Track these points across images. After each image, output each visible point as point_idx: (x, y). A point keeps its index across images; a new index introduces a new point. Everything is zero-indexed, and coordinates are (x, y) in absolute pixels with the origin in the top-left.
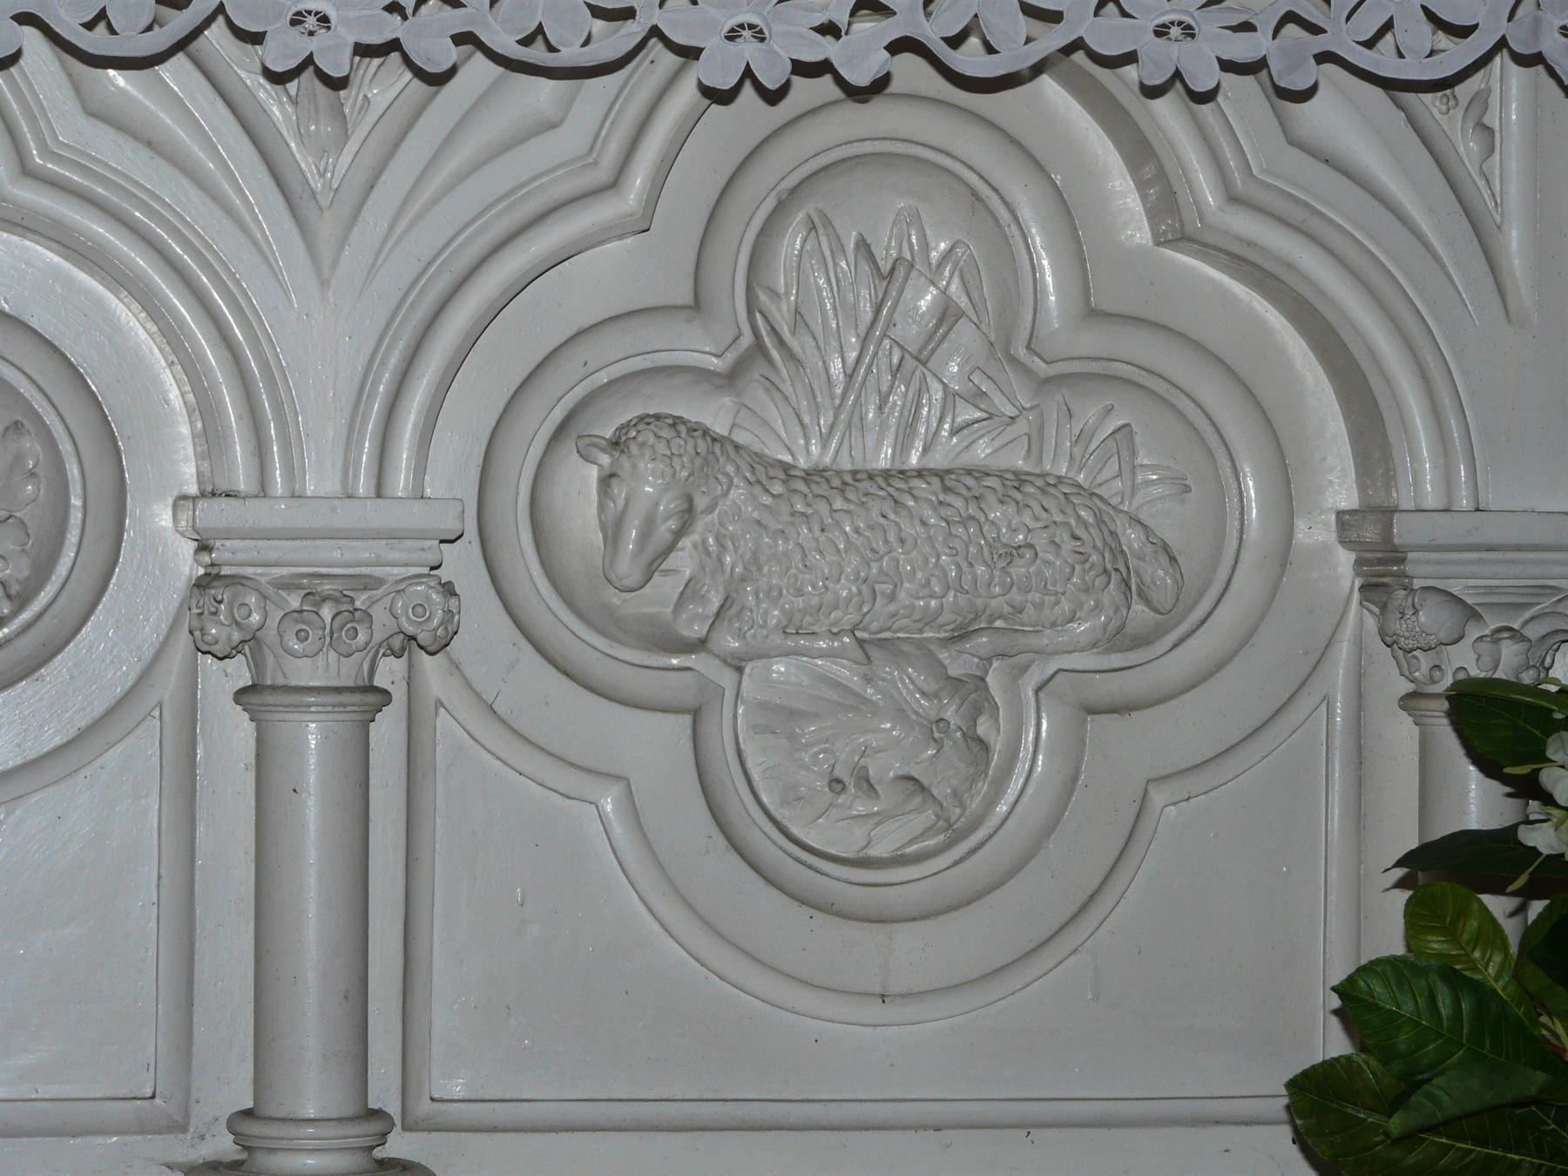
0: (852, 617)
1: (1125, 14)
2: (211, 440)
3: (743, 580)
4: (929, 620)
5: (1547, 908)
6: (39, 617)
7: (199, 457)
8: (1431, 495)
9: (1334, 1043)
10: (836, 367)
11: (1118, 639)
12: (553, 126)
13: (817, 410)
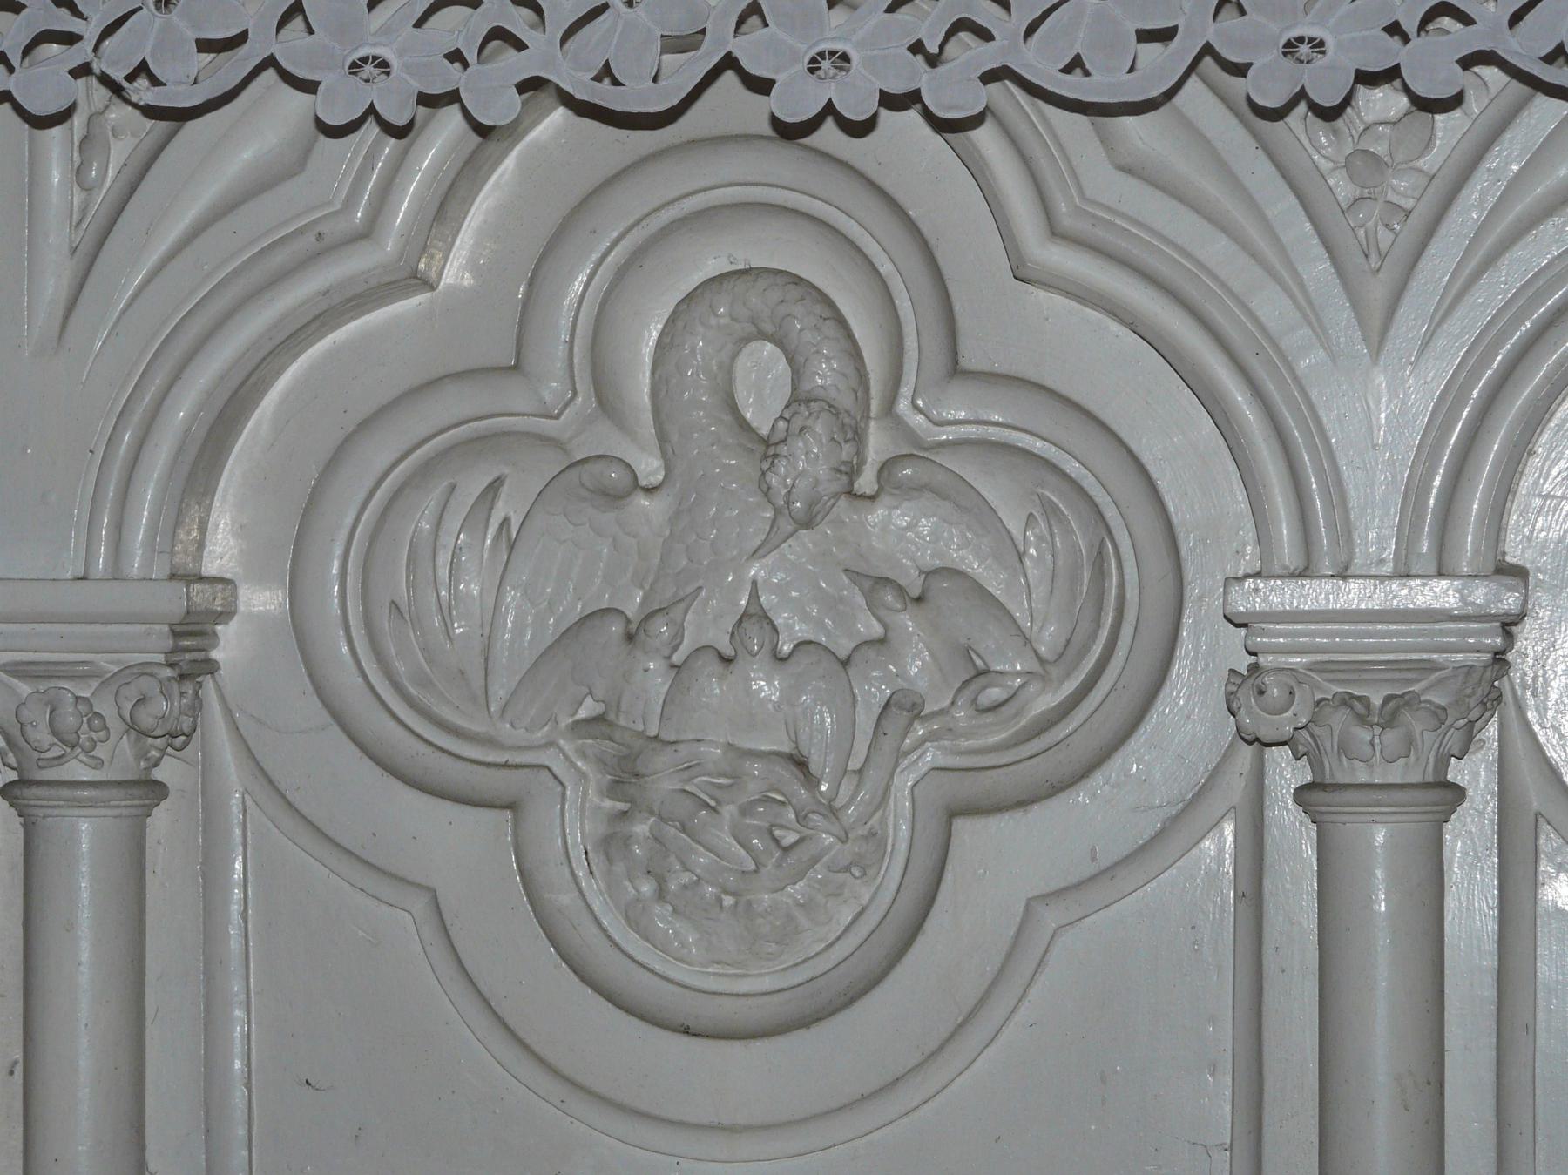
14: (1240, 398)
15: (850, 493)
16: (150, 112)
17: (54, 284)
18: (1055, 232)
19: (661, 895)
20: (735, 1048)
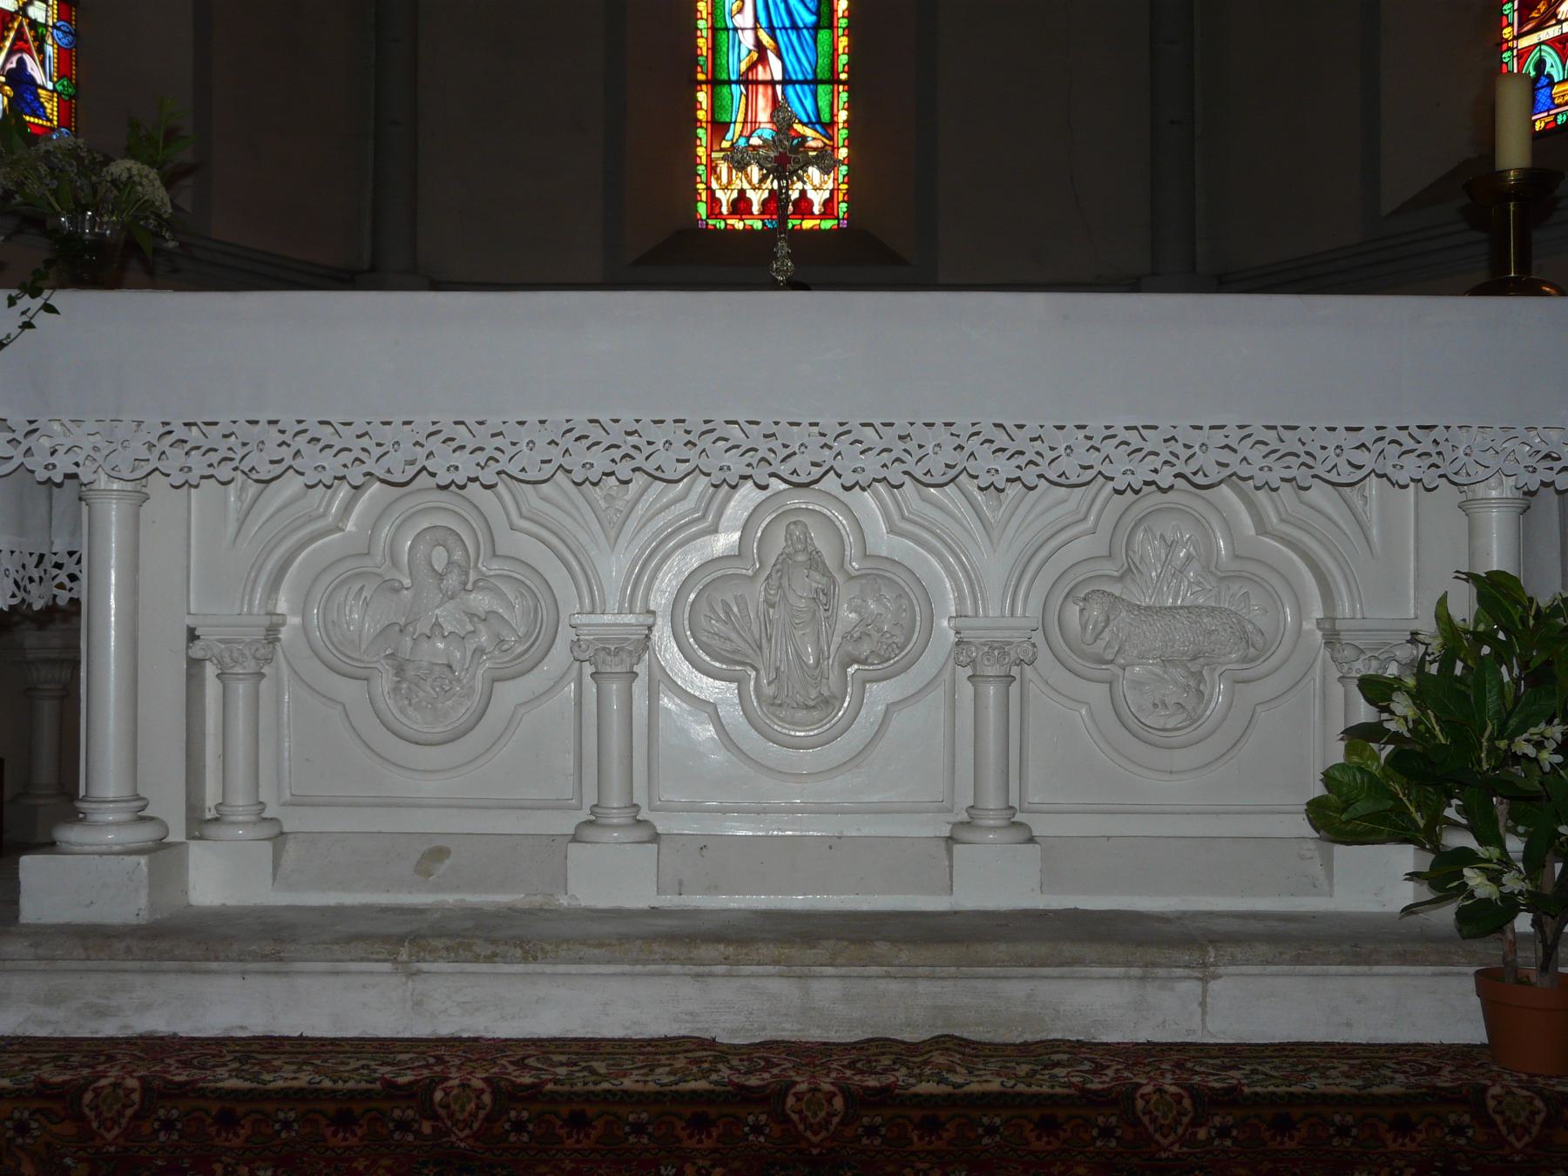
0: (1160, 653)
1: (1249, 464)
2: (960, 599)
3: (1126, 641)
4: (1184, 654)
5: (1394, 749)
6: (907, 654)
7: (956, 605)
8: (1348, 614)
9: (1319, 790)
10: (1154, 574)
11: (1245, 659)
12: (1065, 501)
13: (1148, 588)
14: (574, 563)
15: (465, 590)
16: (257, 481)
17: (231, 529)
18: (522, 516)
19: (410, 704)
20: (433, 748)
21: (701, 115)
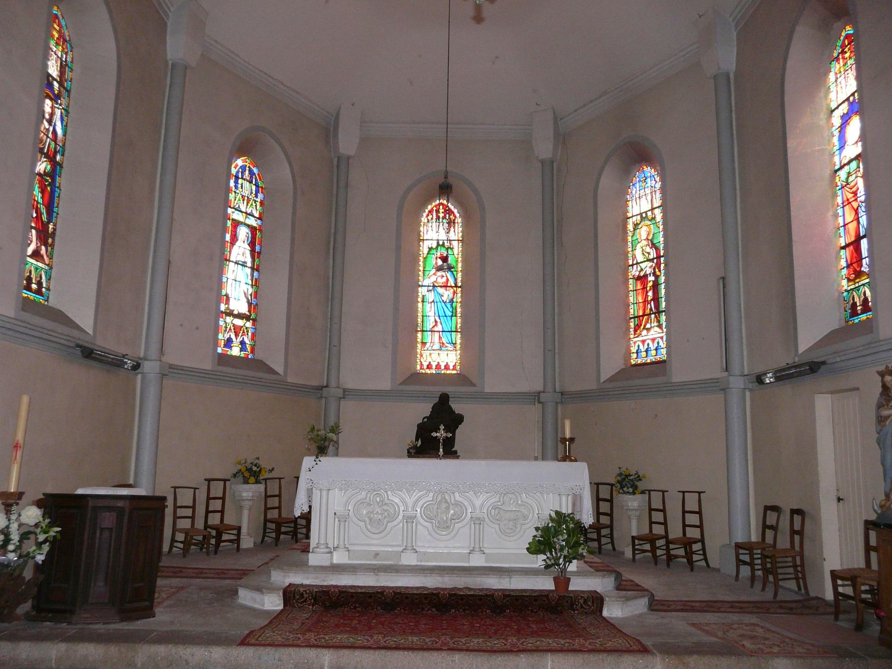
21: (419, 340)
